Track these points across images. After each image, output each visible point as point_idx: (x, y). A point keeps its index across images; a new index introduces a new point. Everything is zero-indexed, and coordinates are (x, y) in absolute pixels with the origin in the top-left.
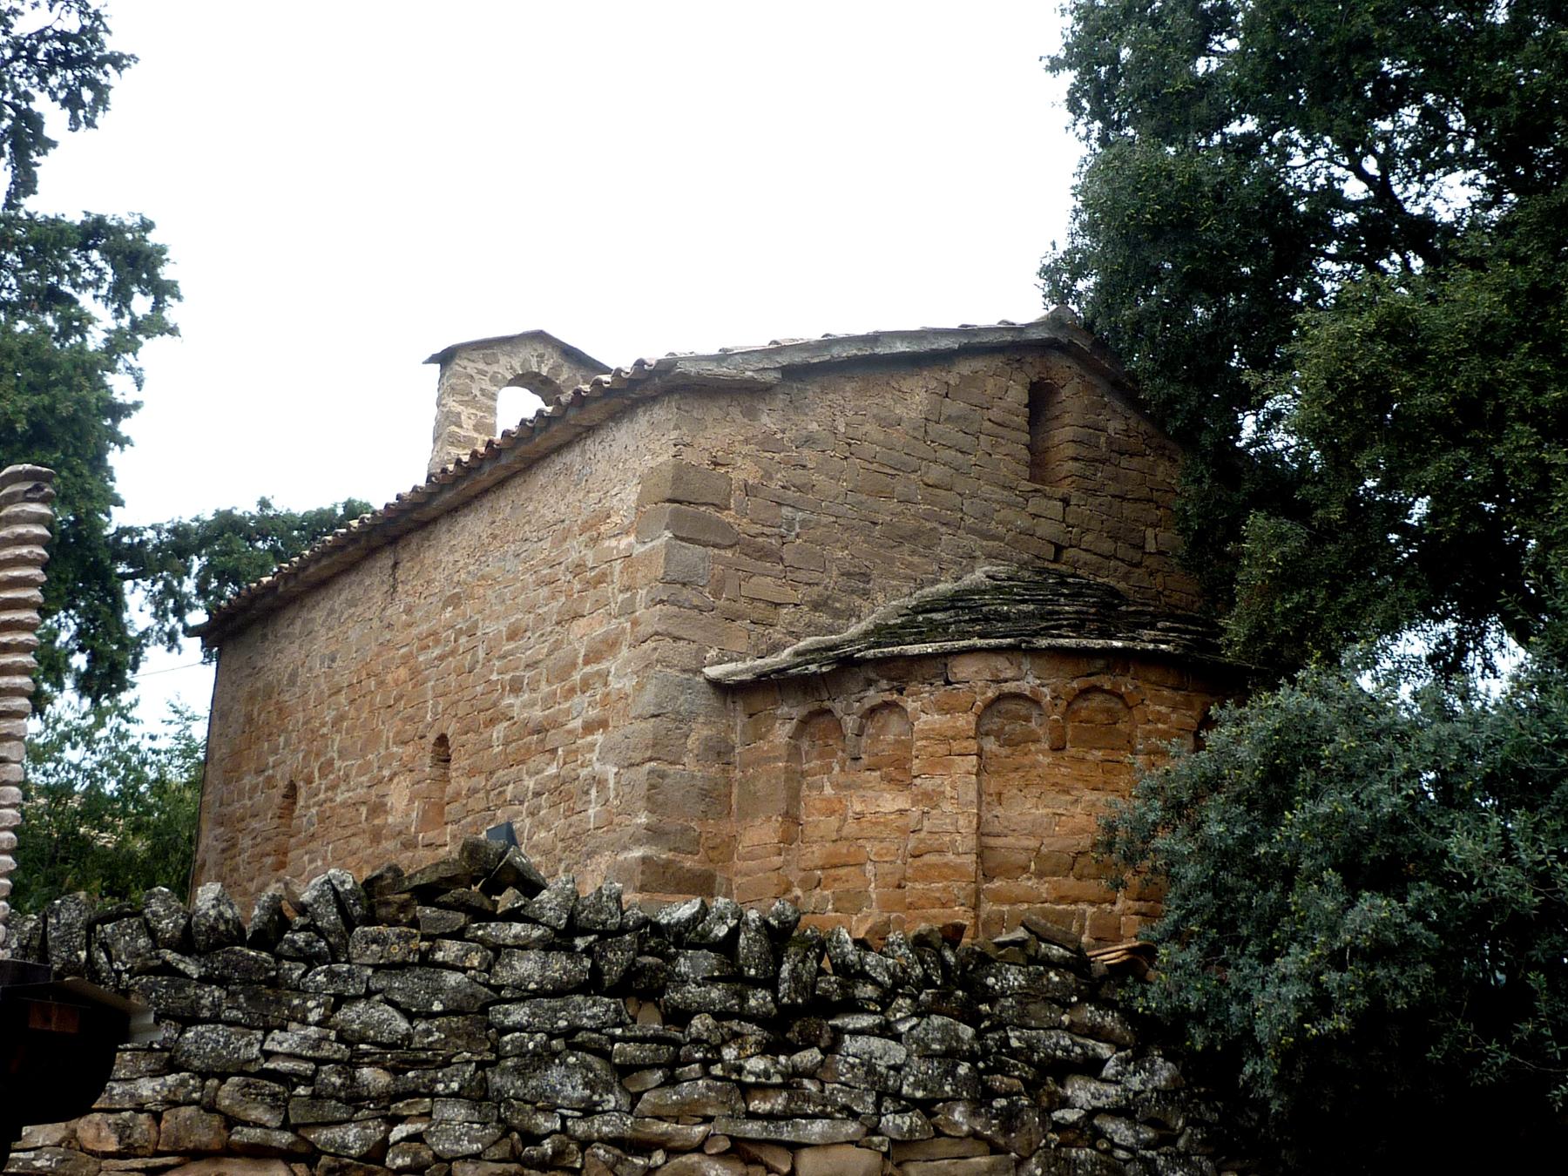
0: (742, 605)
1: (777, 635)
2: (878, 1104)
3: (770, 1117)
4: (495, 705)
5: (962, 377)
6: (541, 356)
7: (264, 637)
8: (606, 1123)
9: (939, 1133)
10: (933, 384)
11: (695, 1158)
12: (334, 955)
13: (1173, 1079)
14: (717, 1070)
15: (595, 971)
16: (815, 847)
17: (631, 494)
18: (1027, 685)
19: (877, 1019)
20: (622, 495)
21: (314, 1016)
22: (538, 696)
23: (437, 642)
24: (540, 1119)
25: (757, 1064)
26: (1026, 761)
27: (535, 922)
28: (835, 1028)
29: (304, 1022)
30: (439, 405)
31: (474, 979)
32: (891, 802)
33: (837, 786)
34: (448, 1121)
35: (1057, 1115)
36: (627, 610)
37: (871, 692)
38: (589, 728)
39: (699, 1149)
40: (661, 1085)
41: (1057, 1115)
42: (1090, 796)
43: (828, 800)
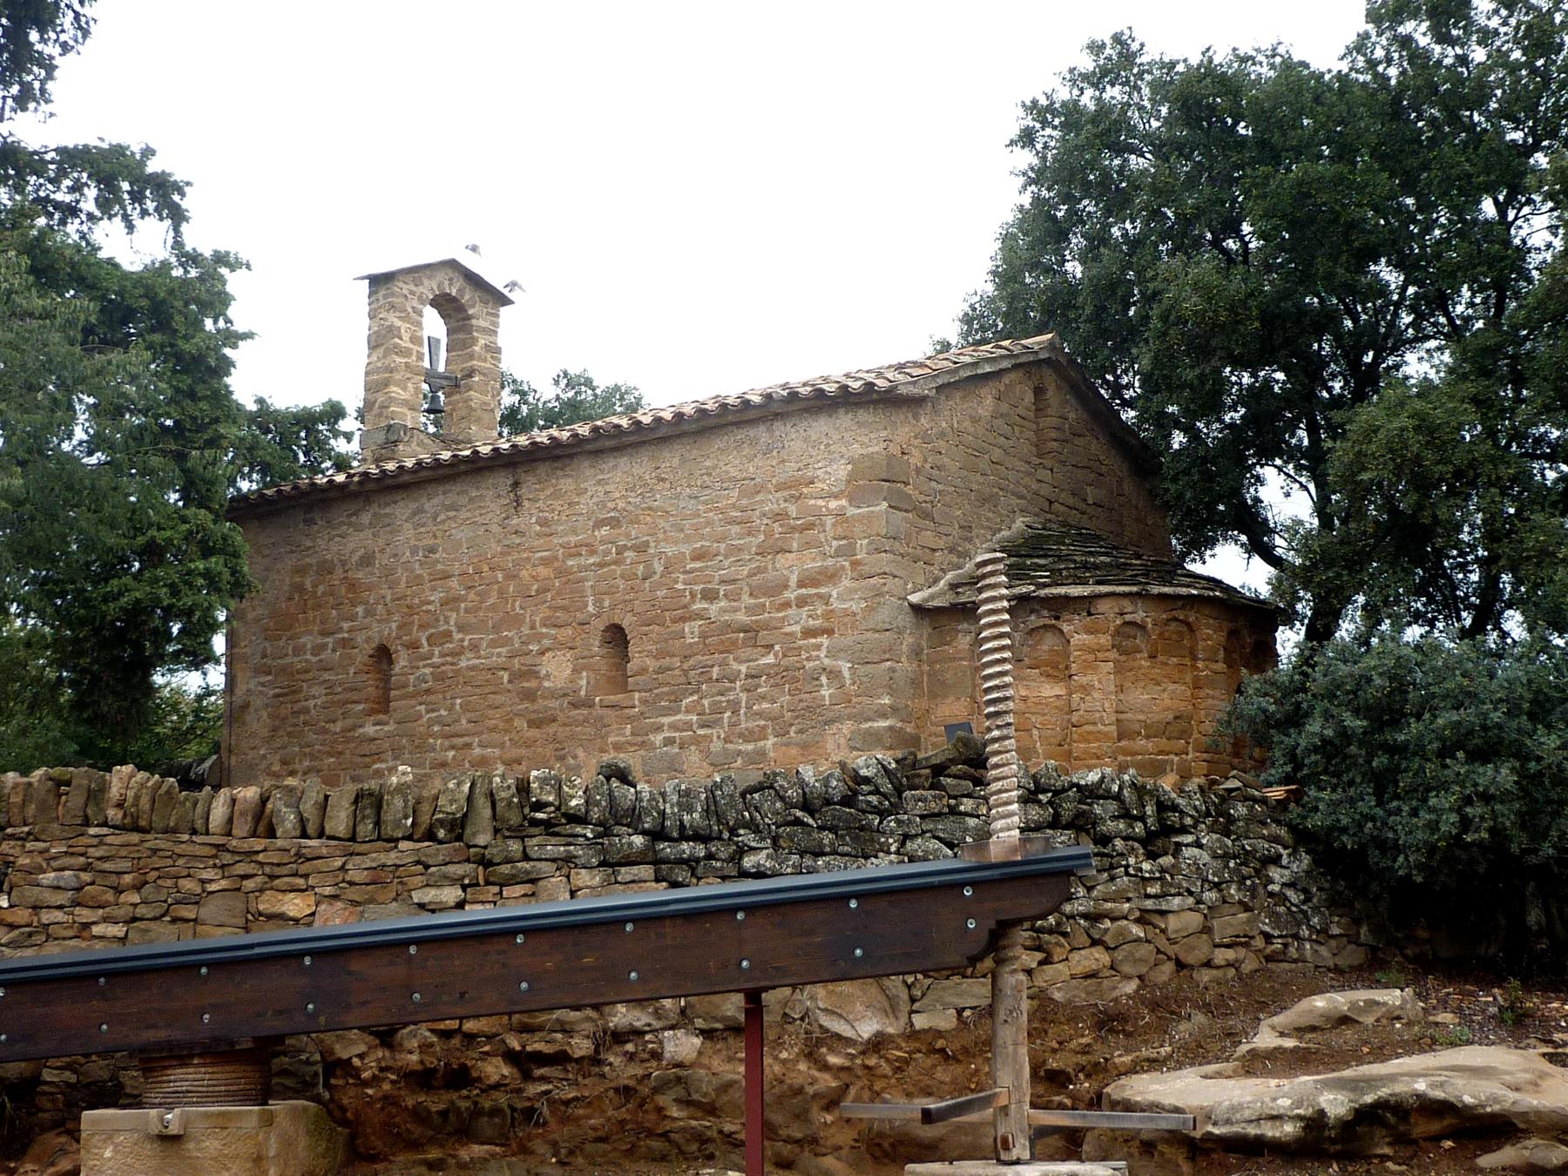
0: (919, 552)
3: (1156, 897)
4: (685, 607)
7: (312, 522)
9: (1225, 902)
12: (895, 809)
15: (1056, 815)
18: (1139, 616)
21: (893, 849)
23: (593, 552)
25: (1146, 866)
26: (1136, 664)
29: (888, 853)
30: (372, 316)
32: (1050, 690)
37: (1033, 617)
39: (1126, 918)
42: (1172, 687)
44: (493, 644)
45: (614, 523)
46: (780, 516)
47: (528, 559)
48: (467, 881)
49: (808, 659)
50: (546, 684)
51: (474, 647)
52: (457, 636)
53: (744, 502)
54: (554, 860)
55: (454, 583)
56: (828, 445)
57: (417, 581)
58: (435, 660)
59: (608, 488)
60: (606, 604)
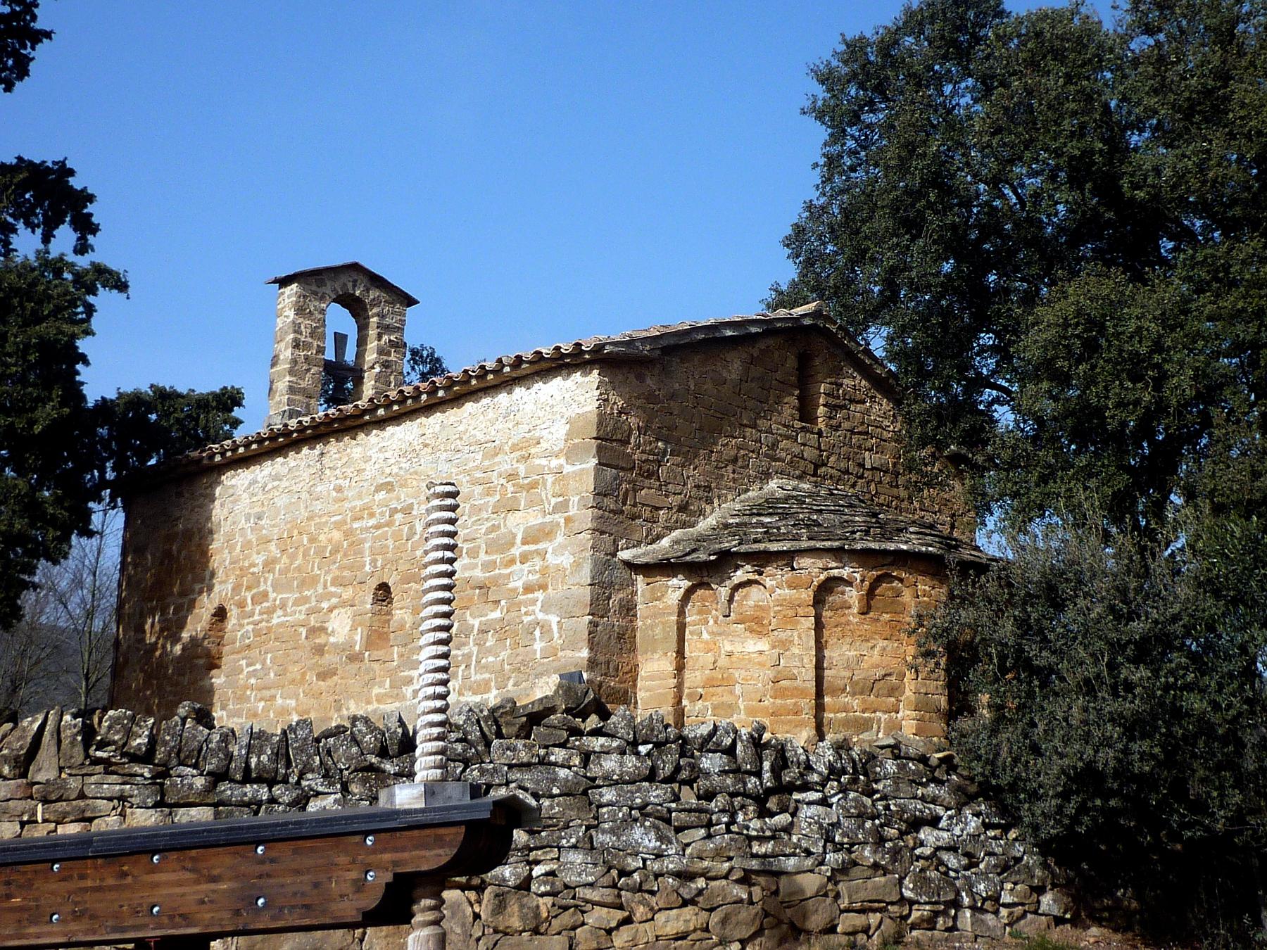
1: (657, 529)
2: (824, 847)
5: (761, 350)
6: (355, 281)
7: (180, 495)
8: (672, 862)
10: (744, 356)
11: (724, 882)
13: (977, 828)
14: (734, 828)
15: (653, 770)
16: (698, 673)
17: (561, 430)
18: (845, 572)
19: (819, 795)
20: (552, 430)
22: (479, 561)
23: (372, 515)
24: (629, 860)
26: (843, 620)
27: (613, 736)
28: (797, 801)
31: (576, 773)
33: (711, 633)
34: (572, 863)
35: (918, 852)
36: (562, 507)
38: (529, 589)
39: (726, 877)
40: (704, 838)
41: (918, 852)
43: (707, 643)
44: (297, 602)
45: (388, 487)
46: (512, 476)
47: (327, 522)
48: (25, 818)
49: (526, 613)
50: (332, 639)
51: (283, 606)
52: (272, 595)
53: (486, 463)
54: (110, 799)
55: (273, 547)
56: (552, 407)
57: (247, 545)
58: (256, 617)
59: (387, 455)
60: (379, 564)
